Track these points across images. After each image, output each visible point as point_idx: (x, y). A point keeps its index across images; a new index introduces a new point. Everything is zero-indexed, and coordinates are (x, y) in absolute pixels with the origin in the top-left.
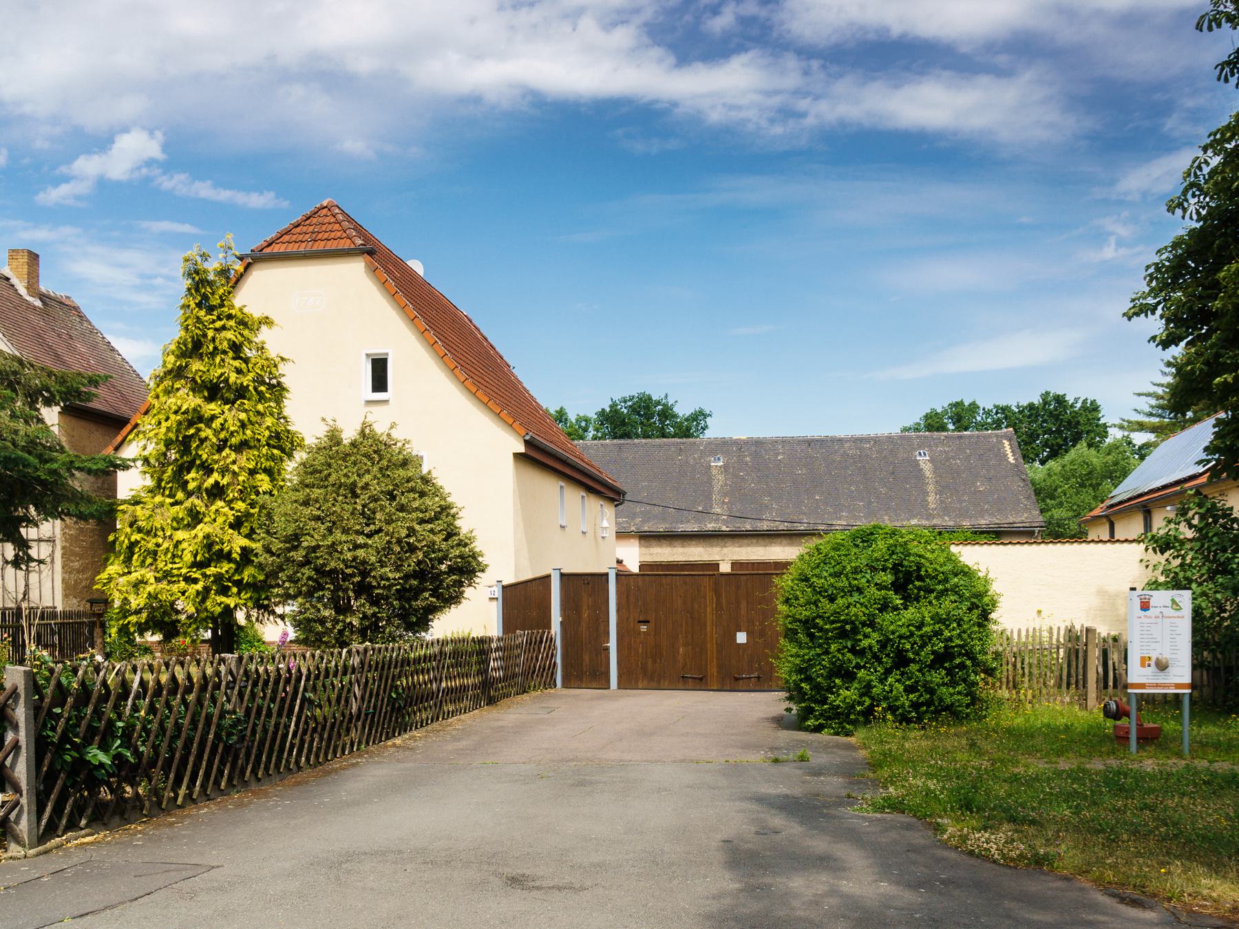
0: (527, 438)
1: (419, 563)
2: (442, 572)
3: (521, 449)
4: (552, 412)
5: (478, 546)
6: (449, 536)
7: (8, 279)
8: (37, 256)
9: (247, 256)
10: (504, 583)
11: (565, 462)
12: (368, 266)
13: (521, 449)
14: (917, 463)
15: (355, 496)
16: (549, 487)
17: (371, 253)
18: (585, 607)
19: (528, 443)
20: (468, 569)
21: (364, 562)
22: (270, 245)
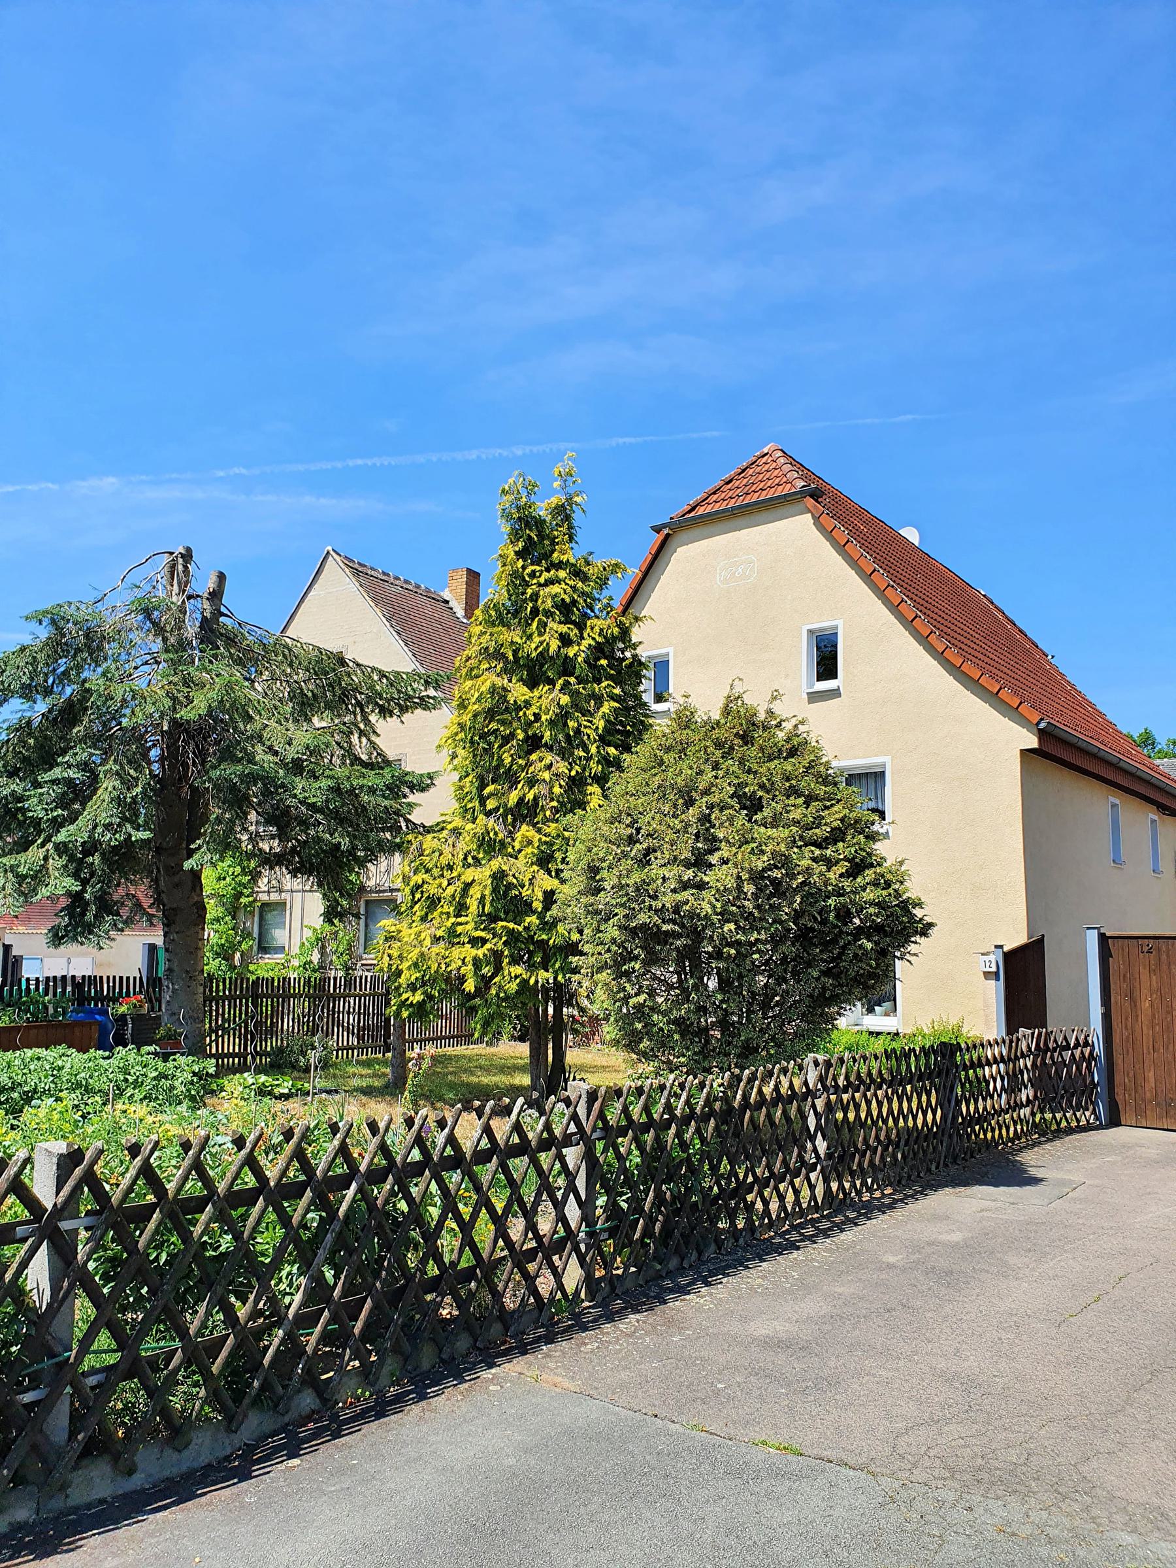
0: (1042, 725)
1: (797, 915)
2: (852, 939)
3: (1033, 742)
4: (1136, 736)
5: (912, 889)
6: (857, 867)
7: (447, 602)
8: (479, 575)
9: (664, 526)
10: (1006, 949)
11: (1115, 766)
12: (817, 520)
13: (1033, 742)
14: (110, 1293)
15: (690, 803)
16: (1094, 805)
17: (816, 495)
18: (1145, 992)
19: (1042, 734)
20: (900, 925)
21: (693, 915)
22: (693, 509)
